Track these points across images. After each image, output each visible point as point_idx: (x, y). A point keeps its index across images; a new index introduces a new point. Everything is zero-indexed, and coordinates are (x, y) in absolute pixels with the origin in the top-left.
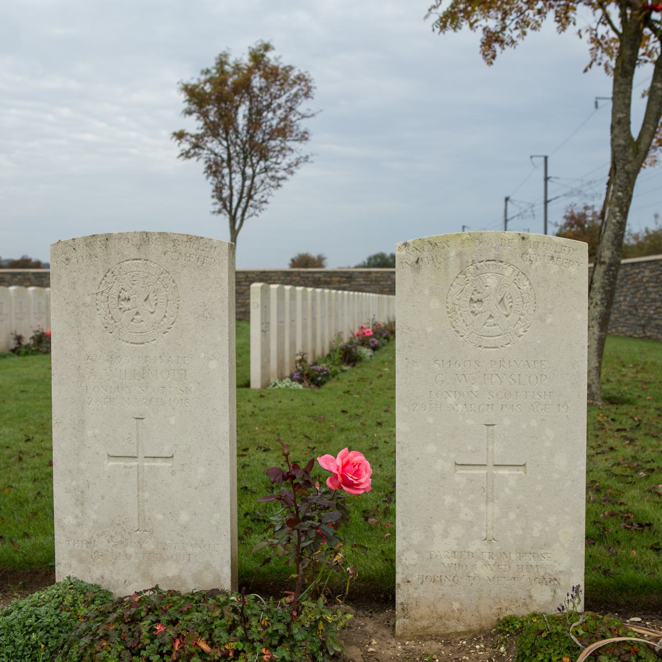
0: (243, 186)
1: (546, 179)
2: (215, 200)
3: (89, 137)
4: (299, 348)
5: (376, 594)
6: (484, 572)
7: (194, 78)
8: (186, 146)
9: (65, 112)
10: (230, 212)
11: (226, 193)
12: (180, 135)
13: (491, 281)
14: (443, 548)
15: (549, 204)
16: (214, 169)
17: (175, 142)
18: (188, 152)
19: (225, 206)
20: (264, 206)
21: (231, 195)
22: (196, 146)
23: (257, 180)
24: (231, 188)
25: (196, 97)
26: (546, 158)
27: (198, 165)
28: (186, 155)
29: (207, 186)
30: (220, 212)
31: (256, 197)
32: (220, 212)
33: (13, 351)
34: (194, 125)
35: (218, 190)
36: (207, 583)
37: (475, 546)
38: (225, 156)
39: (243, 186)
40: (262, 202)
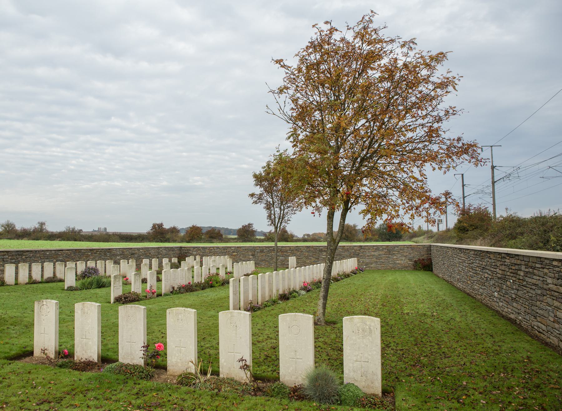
0: (280, 213)
1: (463, 185)
2: (268, 220)
3: (245, 166)
4: (250, 298)
5: (165, 368)
6: (180, 365)
7: (259, 170)
8: (255, 199)
9: (234, 154)
10: (275, 225)
11: (273, 217)
12: (252, 195)
13: (180, 317)
14: (174, 360)
15: (495, 184)
16: (269, 207)
17: (250, 198)
18: (256, 201)
19: (272, 223)
20: (289, 222)
21: (275, 217)
22: (259, 199)
23: (286, 211)
24: (274, 215)
25: (259, 179)
27: (261, 206)
28: (255, 202)
29: (265, 213)
30: (271, 225)
32: (271, 225)
33: (171, 292)
34: (258, 190)
35: (269, 216)
36: (370, 391)
37: (178, 361)
38: (271, 203)
39: (280, 213)
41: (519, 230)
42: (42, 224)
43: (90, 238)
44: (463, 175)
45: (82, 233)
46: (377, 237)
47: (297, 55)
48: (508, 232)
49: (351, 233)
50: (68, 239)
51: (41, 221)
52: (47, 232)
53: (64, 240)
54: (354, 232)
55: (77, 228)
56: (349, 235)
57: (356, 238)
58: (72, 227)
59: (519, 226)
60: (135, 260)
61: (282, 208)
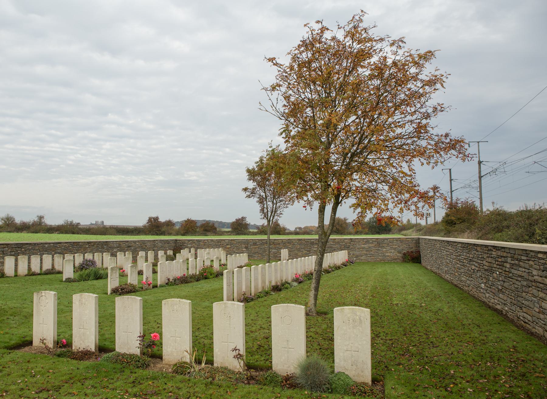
0: (273, 207)
1: (451, 180)
2: (261, 214)
4: (244, 289)
5: (160, 357)
7: (252, 165)
8: (248, 193)
10: (267, 218)
11: (265, 211)
12: (245, 190)
13: (175, 307)
16: (262, 201)
17: (243, 193)
18: (249, 195)
19: (265, 216)
20: (281, 215)
21: (268, 211)
22: (252, 193)
24: (267, 208)
25: (252, 174)
26: (450, 170)
27: (254, 201)
28: (249, 196)
29: (258, 207)
31: (278, 212)
33: (167, 284)
34: (251, 185)
35: (262, 210)
37: (174, 350)
39: (273, 207)
40: (280, 214)
41: (505, 223)
42: (41, 218)
43: (88, 231)
45: (80, 227)
46: (367, 230)
47: (289, 54)
48: (494, 225)
49: (341, 226)
50: (66, 232)
51: (40, 215)
52: (46, 225)
53: (62, 233)
54: (344, 225)
55: (75, 221)
56: (340, 228)
57: (346, 231)
58: (70, 220)
59: (506, 220)
60: (131, 253)
61: (275, 202)
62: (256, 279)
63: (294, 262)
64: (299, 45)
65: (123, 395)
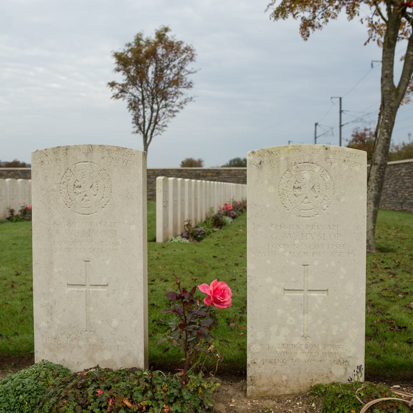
0: (152, 116)
1: (341, 112)
2: (134, 125)
3: (55, 85)
5: (235, 370)
6: (302, 357)
7: (121, 48)
8: (116, 91)
10: (143, 132)
11: (141, 120)
12: (112, 84)
13: (306, 175)
15: (342, 127)
16: (133, 106)
17: (109, 89)
18: (117, 95)
19: (140, 129)
20: (165, 128)
21: (144, 122)
23: (160, 112)
24: (144, 117)
25: (122, 61)
27: (123, 103)
28: (116, 96)
29: (129, 116)
30: (137, 132)
32: (137, 132)
33: (8, 219)
34: (121, 78)
35: (136, 118)
36: (129, 364)
37: (297, 341)
38: (140, 98)
40: (163, 126)
44: (341, 99)
61: (155, 107)
62: (183, 215)
63: (187, 185)
64: (333, 18)
65: (377, 321)
